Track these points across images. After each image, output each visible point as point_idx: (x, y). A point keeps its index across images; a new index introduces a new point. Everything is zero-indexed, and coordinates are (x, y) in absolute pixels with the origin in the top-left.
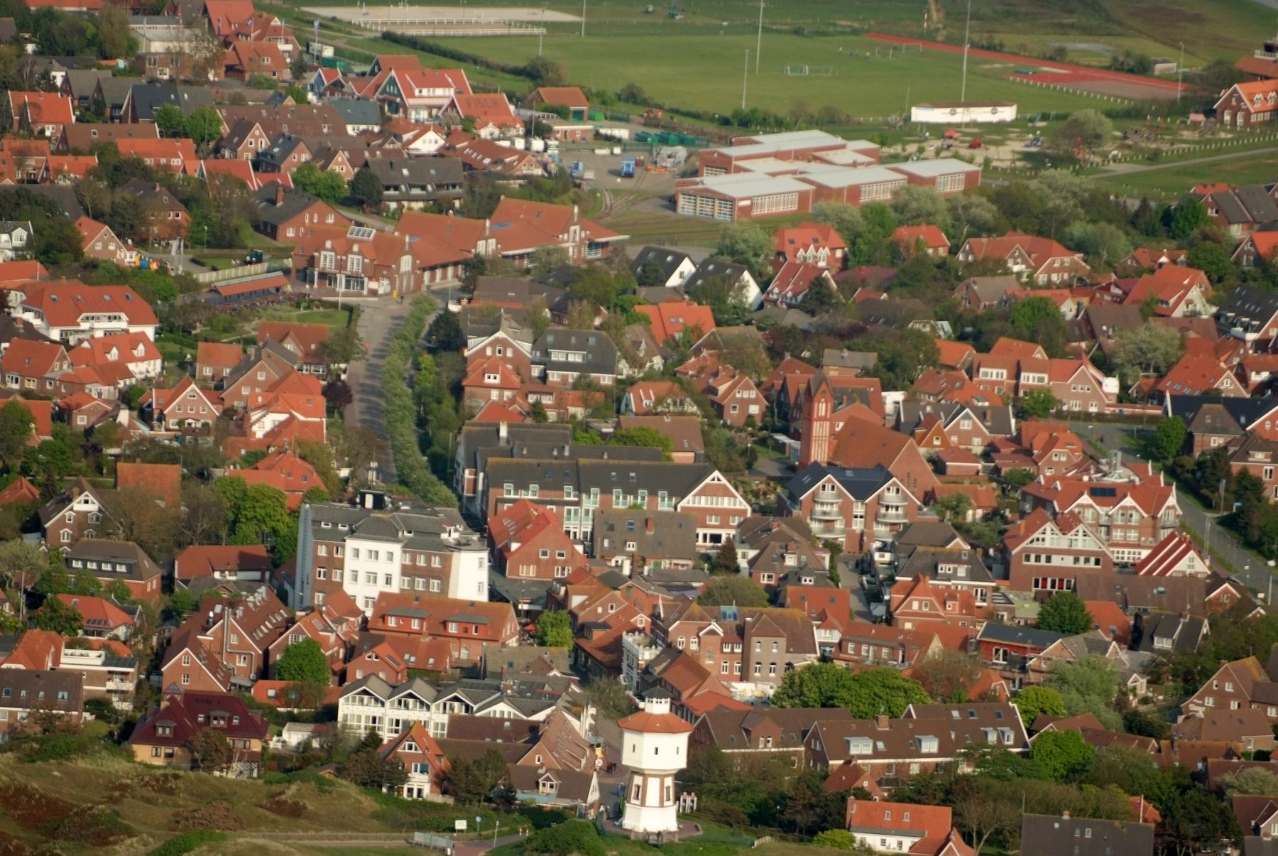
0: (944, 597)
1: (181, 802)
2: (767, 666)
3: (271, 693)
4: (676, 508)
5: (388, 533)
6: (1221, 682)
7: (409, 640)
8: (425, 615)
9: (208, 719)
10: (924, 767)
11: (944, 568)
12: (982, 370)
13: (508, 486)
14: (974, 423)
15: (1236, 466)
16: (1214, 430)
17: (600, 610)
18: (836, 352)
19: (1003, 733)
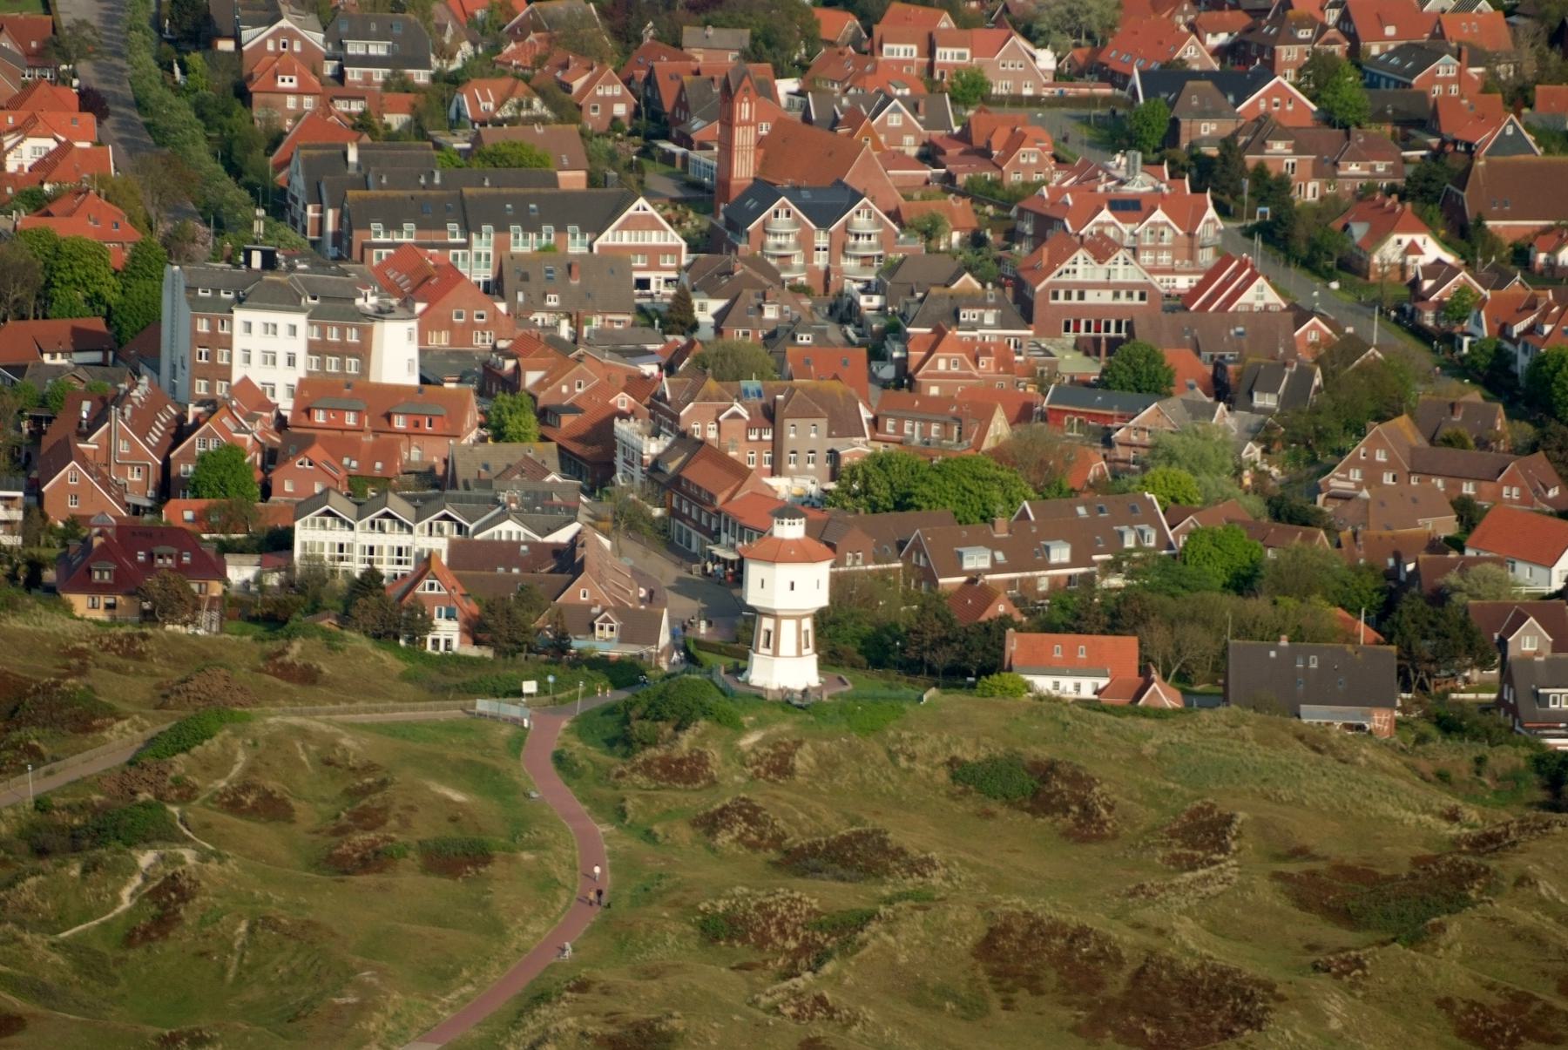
0: (976, 352)
1: (158, 670)
2: (803, 455)
3: (188, 515)
4: (591, 248)
5: (286, 300)
6: (1371, 449)
7: (342, 433)
8: (362, 406)
9: (151, 556)
10: (1054, 581)
11: (967, 315)
12: (886, 46)
13: (376, 226)
14: (905, 117)
15: (1251, 159)
16: (1204, 115)
18: (699, 30)
19: (1142, 532)
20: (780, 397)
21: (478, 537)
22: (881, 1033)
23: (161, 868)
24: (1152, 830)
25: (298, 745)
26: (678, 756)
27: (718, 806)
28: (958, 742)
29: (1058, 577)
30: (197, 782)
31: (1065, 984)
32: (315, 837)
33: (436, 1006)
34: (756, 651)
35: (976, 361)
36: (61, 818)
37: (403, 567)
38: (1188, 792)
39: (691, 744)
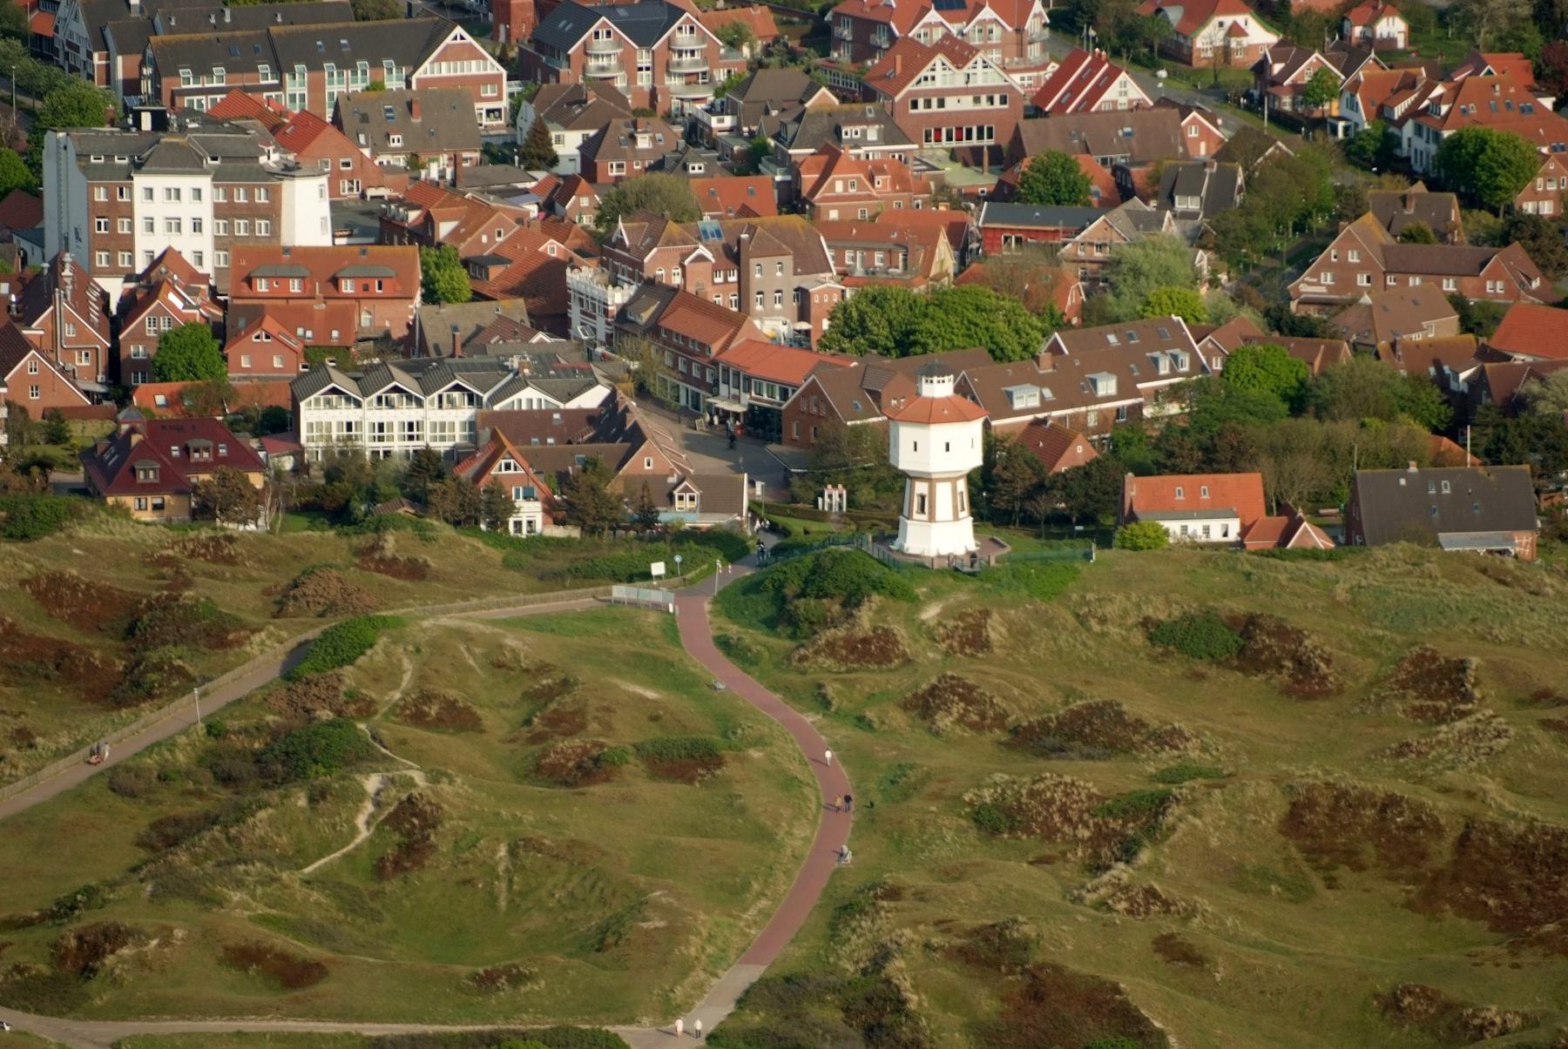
3: (160, 399)
4: (409, 84)
5: (187, 162)
6: (1343, 250)
8: (306, 273)
9: (186, 450)
13: (185, 72)
17: (484, 239)
19: (1175, 357)
20: (744, 236)
21: (497, 408)
22: (1223, 924)
23: (393, 793)
24: (1376, 682)
25: (462, 648)
26: (861, 635)
27: (925, 686)
28: (1148, 601)
29: (1108, 410)
30: (374, 695)
31: (1387, 859)
32: (513, 746)
33: (742, 924)
34: (909, 517)
35: (872, 180)
36: (238, 742)
37: (415, 443)
38: (1399, 639)
39: (871, 620)
